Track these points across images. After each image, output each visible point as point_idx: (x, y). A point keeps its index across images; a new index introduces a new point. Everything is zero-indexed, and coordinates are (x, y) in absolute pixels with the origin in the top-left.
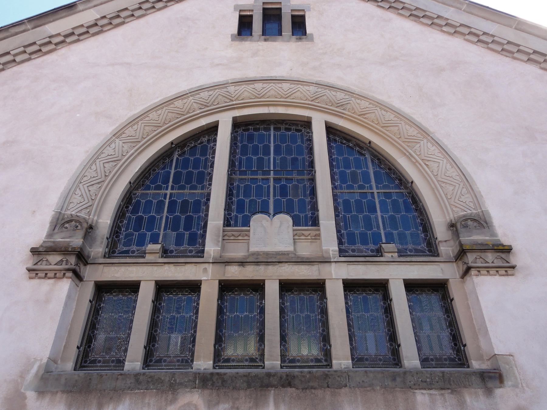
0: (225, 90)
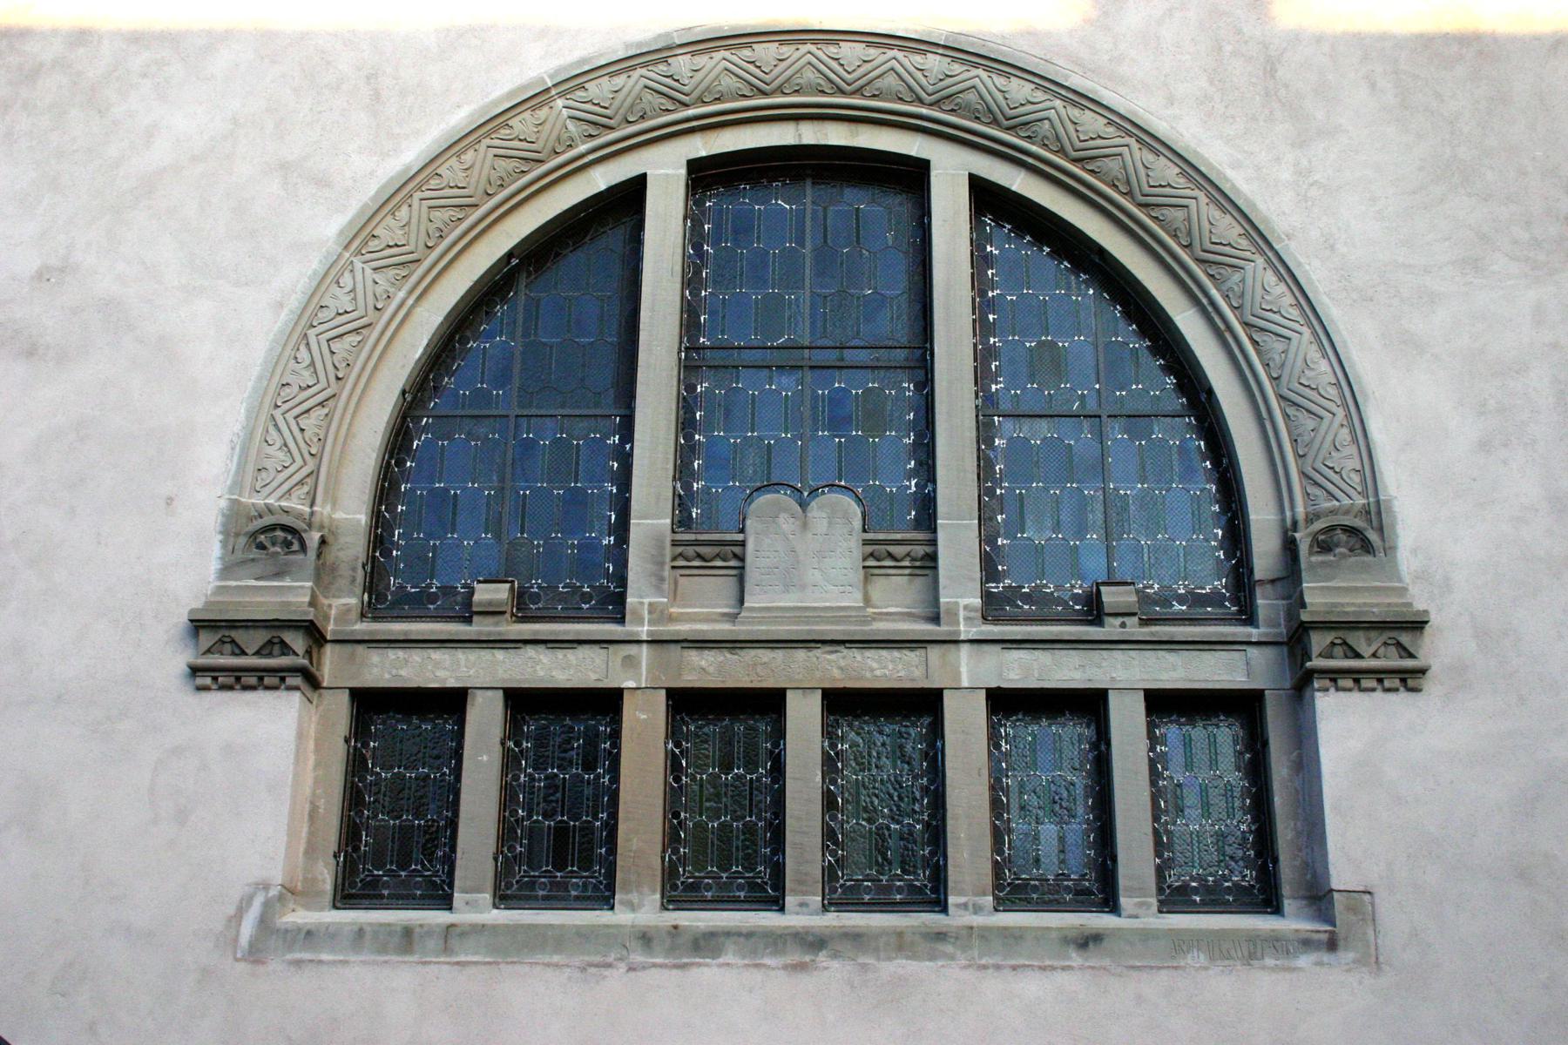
0: (662, 67)
